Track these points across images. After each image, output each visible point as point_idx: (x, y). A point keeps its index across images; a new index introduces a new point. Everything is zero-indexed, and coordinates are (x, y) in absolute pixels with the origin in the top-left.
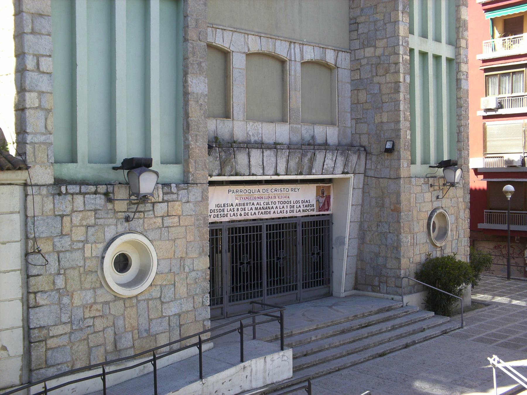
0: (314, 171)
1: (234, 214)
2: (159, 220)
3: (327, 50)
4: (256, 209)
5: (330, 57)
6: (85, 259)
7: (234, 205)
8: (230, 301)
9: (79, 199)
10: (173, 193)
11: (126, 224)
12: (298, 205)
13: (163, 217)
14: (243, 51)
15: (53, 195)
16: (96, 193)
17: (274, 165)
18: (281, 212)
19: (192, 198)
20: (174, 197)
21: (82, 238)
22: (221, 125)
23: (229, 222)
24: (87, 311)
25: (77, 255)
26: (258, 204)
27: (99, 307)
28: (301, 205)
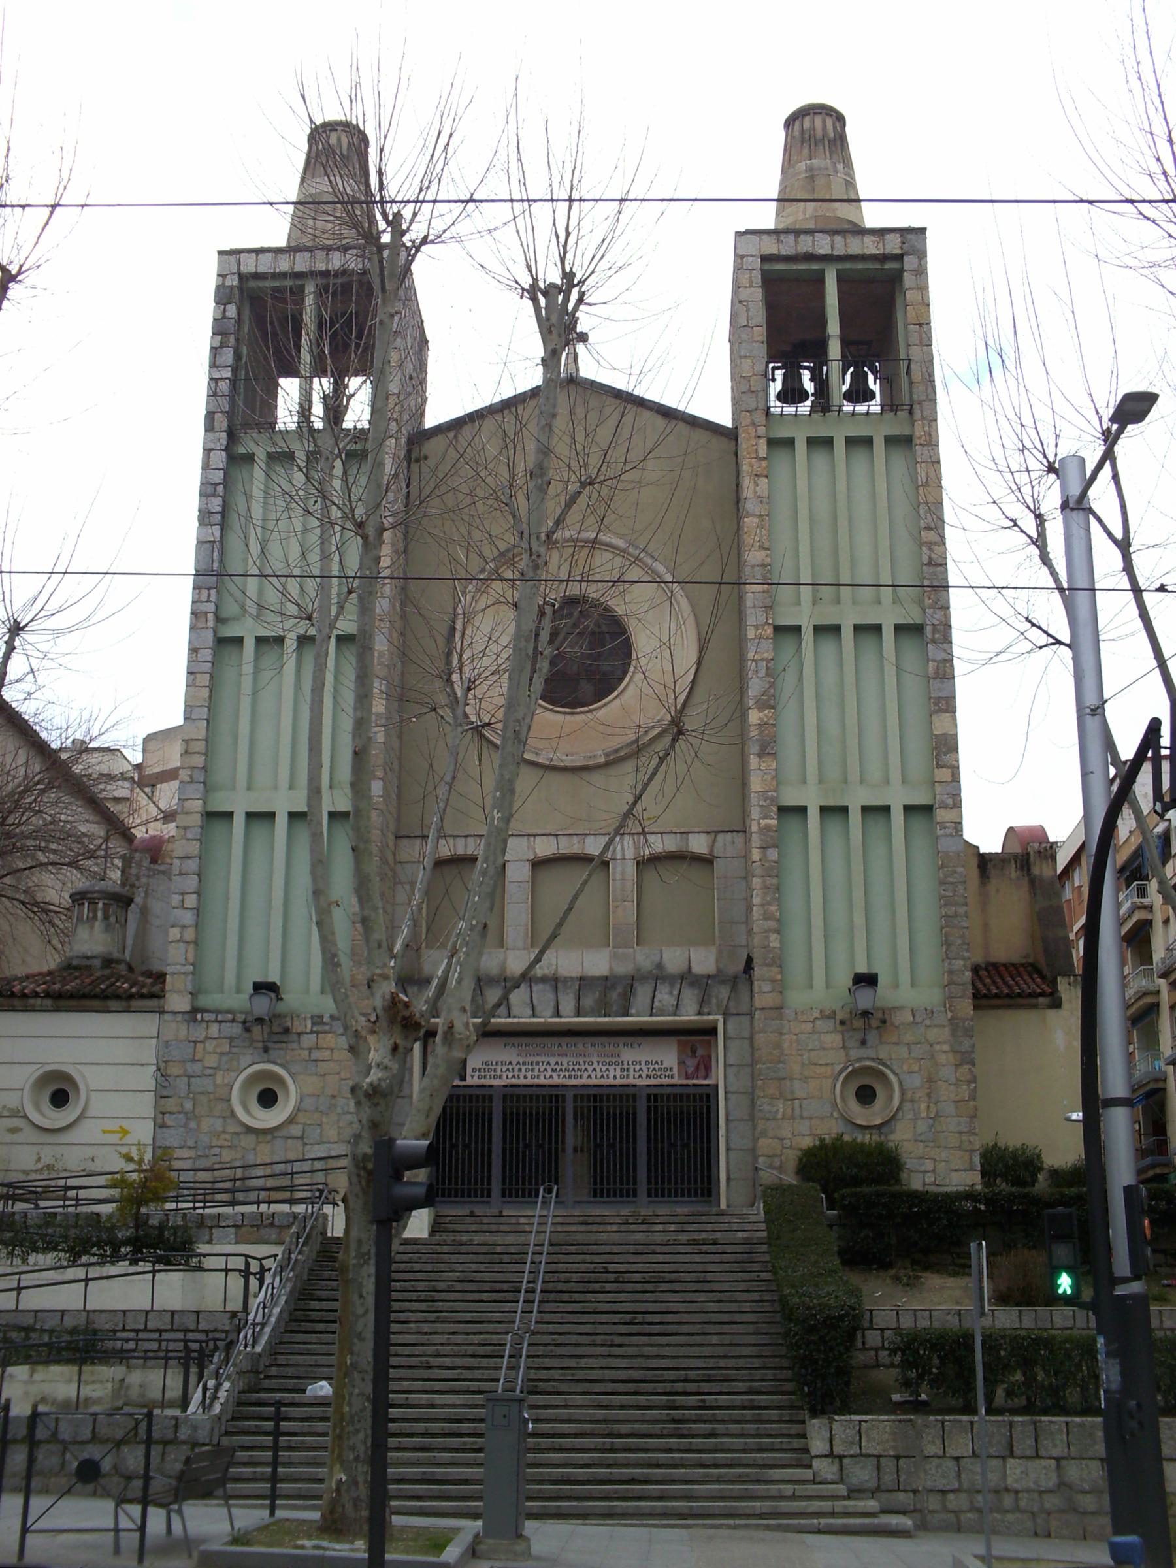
0: (633, 1011)
1: (514, 1076)
2: (306, 1053)
4: (553, 1070)
5: (698, 844)
6: (215, 1085)
7: (514, 1063)
8: (503, 1195)
9: (214, 1028)
10: (326, 1024)
11: (265, 1055)
12: (637, 1067)
13: (310, 1049)
14: (526, 857)
15: (188, 1022)
16: (233, 1021)
17: (552, 1004)
18: (602, 1076)
20: (327, 1028)
21: (215, 1065)
23: (505, 1086)
26: (557, 1063)
27: (227, 1137)
28: (644, 1068)
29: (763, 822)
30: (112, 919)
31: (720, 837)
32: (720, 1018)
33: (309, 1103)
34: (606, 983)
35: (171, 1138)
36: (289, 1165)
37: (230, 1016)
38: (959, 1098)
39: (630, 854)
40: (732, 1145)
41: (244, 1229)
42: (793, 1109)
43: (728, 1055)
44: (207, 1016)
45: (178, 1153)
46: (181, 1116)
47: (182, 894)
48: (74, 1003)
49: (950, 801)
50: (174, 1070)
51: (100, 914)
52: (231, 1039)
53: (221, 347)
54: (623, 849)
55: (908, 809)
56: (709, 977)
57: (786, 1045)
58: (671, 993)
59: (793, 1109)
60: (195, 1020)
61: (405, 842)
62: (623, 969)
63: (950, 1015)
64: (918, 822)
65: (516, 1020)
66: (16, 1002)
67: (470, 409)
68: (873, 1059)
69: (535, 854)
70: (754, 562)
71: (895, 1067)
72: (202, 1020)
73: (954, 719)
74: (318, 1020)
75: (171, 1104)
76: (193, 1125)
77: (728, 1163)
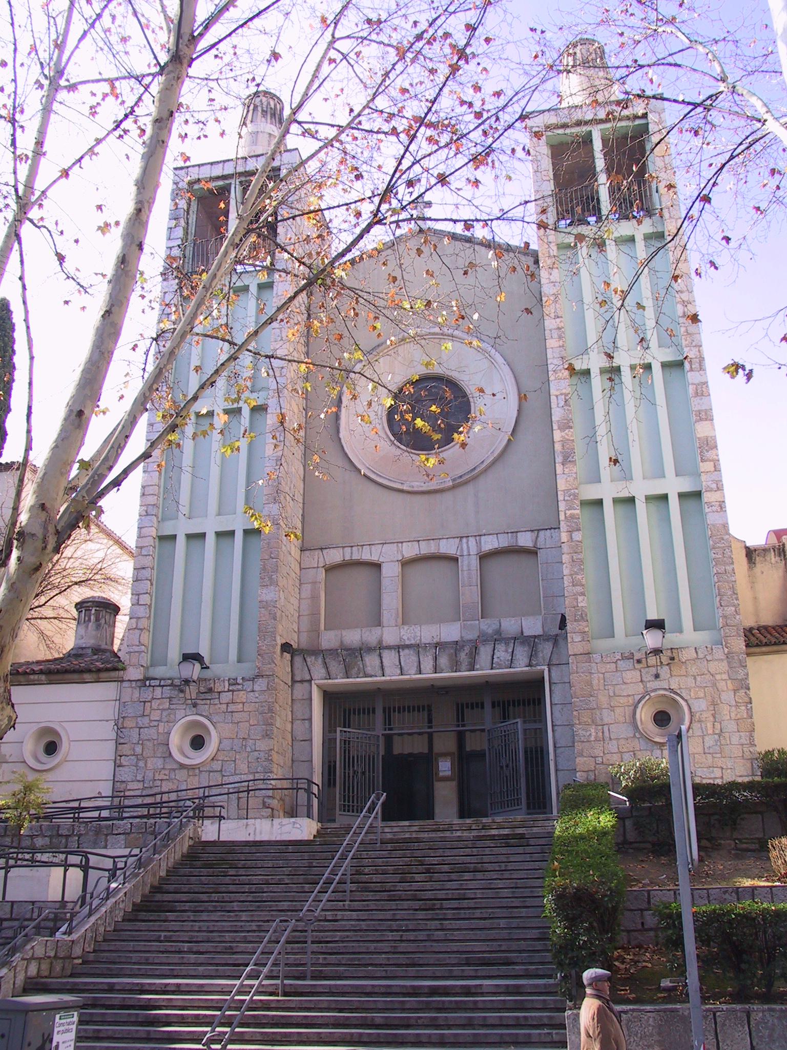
0: (477, 666)
2: (225, 706)
3: (519, 534)
5: (525, 540)
11: (194, 709)
14: (396, 559)
17: (416, 664)
19: (257, 688)
20: (240, 687)
21: (158, 718)
22: (368, 633)
24: (157, 775)
25: (153, 730)
27: (167, 772)
29: (568, 512)
30: (103, 621)
31: (542, 533)
32: (546, 668)
33: (226, 744)
34: (457, 646)
35: (125, 774)
36: (202, 790)
37: (170, 682)
38: (739, 716)
39: (473, 551)
40: (560, 767)
41: (132, 835)
42: (603, 733)
43: (554, 695)
44: (153, 683)
45: (131, 786)
46: (133, 757)
47: (138, 595)
48: (59, 677)
49: (714, 486)
50: (129, 723)
51: (92, 617)
52: (170, 698)
53: (175, 227)
54: (468, 547)
55: (682, 496)
56: (535, 637)
57: (595, 682)
58: (506, 651)
59: (603, 733)
60: (145, 686)
61: (307, 553)
62: (472, 635)
63: (726, 650)
64: (691, 504)
65: (388, 678)
66: (21, 678)
67: (642, 558)
68: (665, 689)
69: (403, 556)
70: (551, 327)
71: (684, 695)
72: (150, 686)
73: (713, 425)
74: (233, 682)
75: (126, 749)
76: (141, 764)
77: (557, 781)
